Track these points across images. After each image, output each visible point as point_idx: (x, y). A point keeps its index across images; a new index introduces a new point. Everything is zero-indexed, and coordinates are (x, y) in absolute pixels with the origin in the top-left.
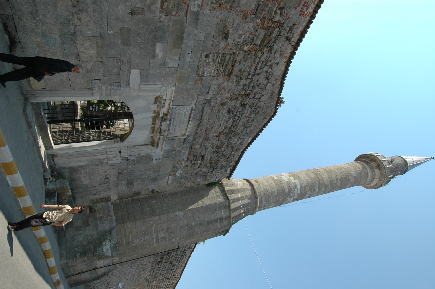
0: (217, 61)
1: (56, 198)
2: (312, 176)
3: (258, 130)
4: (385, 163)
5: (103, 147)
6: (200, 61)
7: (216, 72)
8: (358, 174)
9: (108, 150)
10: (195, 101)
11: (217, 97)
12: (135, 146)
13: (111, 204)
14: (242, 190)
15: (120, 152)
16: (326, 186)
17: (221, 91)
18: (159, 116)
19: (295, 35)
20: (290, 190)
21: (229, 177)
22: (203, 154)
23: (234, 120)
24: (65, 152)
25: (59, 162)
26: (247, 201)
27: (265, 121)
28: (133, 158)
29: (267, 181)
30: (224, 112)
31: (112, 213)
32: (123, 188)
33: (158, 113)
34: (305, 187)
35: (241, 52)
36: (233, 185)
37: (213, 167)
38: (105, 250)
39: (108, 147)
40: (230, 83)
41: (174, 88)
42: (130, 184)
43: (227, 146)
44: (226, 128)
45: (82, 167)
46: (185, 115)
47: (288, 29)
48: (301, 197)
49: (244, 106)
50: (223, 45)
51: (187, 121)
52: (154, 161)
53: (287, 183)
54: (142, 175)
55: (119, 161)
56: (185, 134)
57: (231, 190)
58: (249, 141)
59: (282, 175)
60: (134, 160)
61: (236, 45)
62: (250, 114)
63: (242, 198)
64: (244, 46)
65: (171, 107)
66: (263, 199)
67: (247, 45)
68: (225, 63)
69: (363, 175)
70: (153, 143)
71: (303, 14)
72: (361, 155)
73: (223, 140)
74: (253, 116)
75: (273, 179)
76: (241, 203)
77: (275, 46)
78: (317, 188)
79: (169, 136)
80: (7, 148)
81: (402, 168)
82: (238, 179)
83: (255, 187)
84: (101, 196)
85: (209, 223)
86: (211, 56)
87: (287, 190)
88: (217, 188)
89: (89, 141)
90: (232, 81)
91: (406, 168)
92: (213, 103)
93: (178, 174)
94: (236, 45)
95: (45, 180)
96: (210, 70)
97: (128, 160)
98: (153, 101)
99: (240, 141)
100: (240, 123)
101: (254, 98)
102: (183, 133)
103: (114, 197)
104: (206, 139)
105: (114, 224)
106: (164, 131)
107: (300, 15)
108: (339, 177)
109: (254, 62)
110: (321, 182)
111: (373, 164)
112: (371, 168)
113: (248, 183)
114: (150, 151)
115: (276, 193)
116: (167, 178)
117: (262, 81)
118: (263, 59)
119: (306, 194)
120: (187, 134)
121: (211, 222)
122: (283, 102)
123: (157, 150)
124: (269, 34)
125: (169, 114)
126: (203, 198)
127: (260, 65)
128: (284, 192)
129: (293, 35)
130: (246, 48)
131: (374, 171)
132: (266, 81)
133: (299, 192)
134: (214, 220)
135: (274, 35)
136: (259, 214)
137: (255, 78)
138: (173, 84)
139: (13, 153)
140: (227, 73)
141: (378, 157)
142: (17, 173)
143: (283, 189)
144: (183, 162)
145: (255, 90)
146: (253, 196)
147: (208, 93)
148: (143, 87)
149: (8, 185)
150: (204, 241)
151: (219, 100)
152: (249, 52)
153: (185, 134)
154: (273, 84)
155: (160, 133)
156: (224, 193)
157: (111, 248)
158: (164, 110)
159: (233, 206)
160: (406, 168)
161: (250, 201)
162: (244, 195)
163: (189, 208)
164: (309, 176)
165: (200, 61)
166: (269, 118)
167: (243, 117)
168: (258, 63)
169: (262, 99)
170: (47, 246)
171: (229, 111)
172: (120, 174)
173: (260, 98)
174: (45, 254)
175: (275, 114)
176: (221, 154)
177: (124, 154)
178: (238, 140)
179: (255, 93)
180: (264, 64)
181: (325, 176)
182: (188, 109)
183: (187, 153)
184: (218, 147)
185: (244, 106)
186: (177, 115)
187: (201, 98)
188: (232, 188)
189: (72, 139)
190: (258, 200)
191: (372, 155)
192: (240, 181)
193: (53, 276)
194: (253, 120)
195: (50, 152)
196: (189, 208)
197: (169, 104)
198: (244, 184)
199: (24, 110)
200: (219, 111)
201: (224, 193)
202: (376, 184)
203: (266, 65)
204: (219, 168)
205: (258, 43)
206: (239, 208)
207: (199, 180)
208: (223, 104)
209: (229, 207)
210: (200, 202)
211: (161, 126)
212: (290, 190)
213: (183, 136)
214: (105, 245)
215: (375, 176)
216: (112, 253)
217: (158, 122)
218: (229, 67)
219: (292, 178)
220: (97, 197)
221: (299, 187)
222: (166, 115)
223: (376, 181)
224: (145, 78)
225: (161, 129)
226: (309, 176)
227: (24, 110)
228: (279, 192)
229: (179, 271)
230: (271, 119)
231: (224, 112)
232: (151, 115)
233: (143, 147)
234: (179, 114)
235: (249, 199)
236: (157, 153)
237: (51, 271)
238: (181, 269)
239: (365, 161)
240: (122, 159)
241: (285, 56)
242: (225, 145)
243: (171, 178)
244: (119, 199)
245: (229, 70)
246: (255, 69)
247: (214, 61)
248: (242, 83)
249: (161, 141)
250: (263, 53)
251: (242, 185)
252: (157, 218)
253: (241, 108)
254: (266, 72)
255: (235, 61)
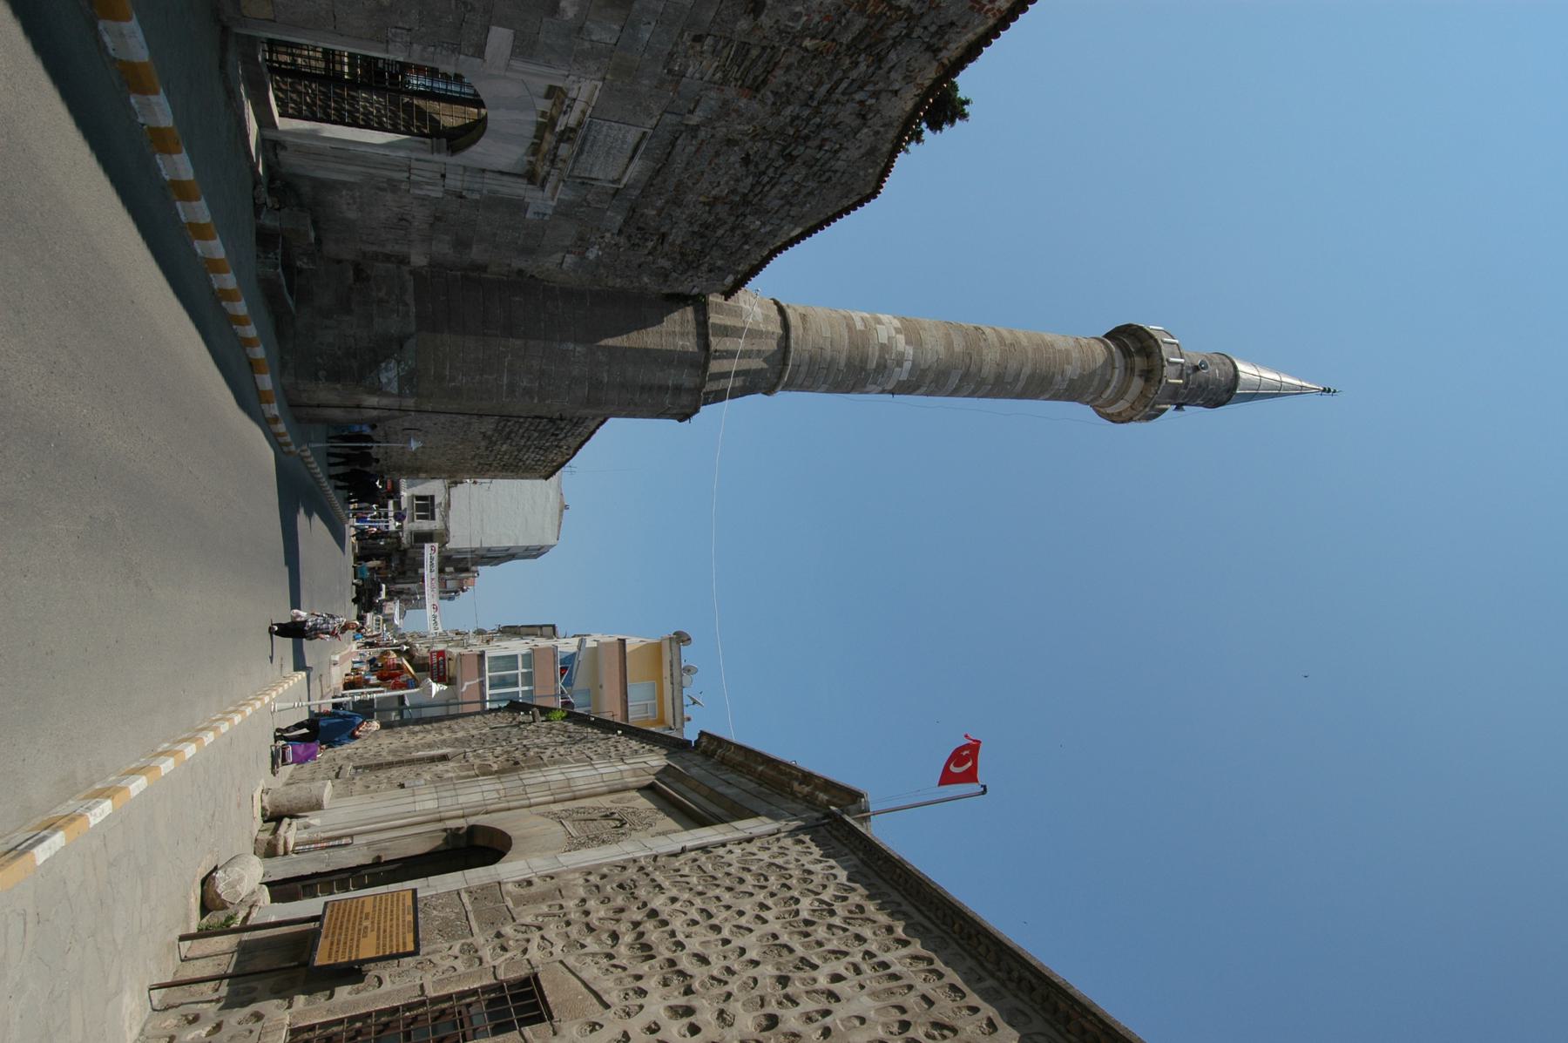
0: (725, 53)
1: (279, 251)
2: (959, 346)
3: (822, 217)
4: (1168, 370)
5: (402, 154)
6: (676, 44)
7: (719, 75)
8: (1081, 377)
9: (414, 164)
10: (654, 121)
11: (717, 124)
12: (484, 171)
13: (411, 273)
14: (754, 334)
15: (443, 176)
16: (982, 382)
17: (728, 115)
18: (554, 125)
19: (952, 46)
20: (882, 367)
21: (729, 294)
22: (663, 230)
23: (758, 183)
24: (306, 142)
25: (288, 159)
26: (757, 364)
27: (846, 203)
28: (477, 196)
29: (832, 327)
30: (732, 159)
31: (410, 298)
32: (443, 248)
33: (553, 122)
34: (924, 372)
35: (794, 49)
36: (737, 313)
37: (688, 262)
38: (384, 380)
39: (414, 155)
40: (755, 105)
41: (600, 84)
42: (462, 244)
43: (733, 229)
44: (733, 192)
45: (344, 184)
46: (623, 142)
47: (933, 29)
48: (906, 388)
49: (790, 159)
50: (744, 24)
51: (629, 153)
52: (529, 215)
53: (883, 347)
54: (495, 235)
55: (440, 195)
56: (618, 181)
57: (726, 327)
58: (794, 234)
59: (879, 322)
60: (477, 201)
61: (780, 32)
62: (806, 178)
63: (746, 354)
64: (803, 38)
65: (587, 120)
66: (804, 369)
67: (813, 37)
68: (747, 63)
69: (1095, 383)
70: (531, 177)
71: (979, 11)
72: (1130, 326)
73: (723, 215)
74: (812, 184)
75: (850, 327)
76: (734, 365)
77: (893, 56)
78: (954, 380)
79: (576, 173)
80: (202, 203)
81: (1217, 390)
82: (753, 304)
83: (793, 335)
84: (388, 249)
85: (644, 388)
86: (709, 41)
87: (872, 365)
88: (689, 313)
89: (368, 126)
90: (762, 101)
91: (1225, 396)
92: (702, 134)
93: (592, 254)
94: (780, 32)
95: (258, 209)
96: (701, 68)
97: (461, 197)
98: (543, 91)
99: (768, 228)
100: (774, 191)
101: (820, 147)
102: (614, 175)
103: (418, 259)
104: (677, 202)
105: (413, 328)
106: (564, 161)
107: (972, 8)
108: (1027, 370)
109: (830, 74)
110: (973, 369)
111: (1139, 362)
112: (1129, 370)
113: (779, 318)
114: (521, 192)
115: (843, 363)
116: (560, 255)
117: (846, 115)
118: (854, 74)
119: (919, 387)
120: (624, 181)
121: (651, 388)
122: (964, 116)
123: (540, 194)
124: (877, 28)
125: (581, 132)
126: (645, 327)
127: (844, 85)
128: (863, 369)
129: (948, 43)
130: (807, 43)
131: (1130, 382)
132: (858, 121)
133: (904, 377)
134: (660, 387)
135: (892, 33)
136: (781, 397)
137: (828, 110)
138: (599, 75)
139: (194, 166)
140: (749, 82)
141: (1163, 347)
142: (129, 19)
143: (864, 360)
144: (608, 235)
145: (826, 134)
146: (779, 356)
147: (691, 112)
148: (516, 64)
149: (196, 254)
150: (943, 108)
151: (721, 131)
152: (817, 53)
153: (618, 181)
154: (877, 133)
155: (553, 162)
156: (703, 330)
157: (400, 378)
158: (571, 119)
159: (715, 366)
160: (1225, 396)
161: (765, 366)
162: (755, 348)
163: (603, 343)
164: (949, 345)
165: (676, 44)
166: (856, 199)
167: (783, 180)
168: (841, 80)
169: (842, 155)
170: (259, 352)
171: (746, 160)
172: (438, 219)
173: (836, 152)
174: (253, 366)
175: (874, 194)
176: (713, 241)
177: (454, 182)
178: (764, 224)
179: (824, 140)
180: (855, 85)
181: (991, 356)
182: (633, 136)
183: (619, 219)
184: (706, 226)
185: (790, 159)
186: (601, 137)
187: (669, 119)
188: (729, 321)
189: (325, 108)
190: (781, 368)
191: (1151, 336)
192: (761, 306)
193: (264, 406)
194: (811, 193)
195: (269, 134)
196: (603, 343)
197: (584, 112)
198: (766, 318)
199: (222, 65)
200: (717, 154)
201: (703, 330)
202: (1120, 414)
203: (861, 88)
204: (705, 268)
205: (846, 39)
206: (726, 375)
207: (646, 280)
208: (730, 142)
209: (705, 367)
210: (634, 335)
211: (556, 148)
212: (882, 367)
213: (613, 182)
214: (387, 370)
215: (1125, 393)
216: (400, 388)
217: (549, 139)
218: (758, 70)
219: (901, 338)
220: (374, 248)
221: (907, 365)
222: (573, 130)
223: (1122, 405)
224: (524, 48)
225: (555, 155)
226: (949, 345)
227: (222, 65)
228: (849, 364)
229: (573, 442)
230: (861, 203)
231: (732, 159)
232: (534, 117)
233: (505, 178)
234: (607, 135)
235: (765, 360)
236: (540, 201)
237: (263, 397)
238: (579, 440)
239: (1126, 346)
240: (446, 192)
241: (919, 81)
242: (727, 227)
243: (570, 259)
244: (430, 265)
245: (756, 78)
246: (830, 91)
247: (715, 52)
248: (788, 111)
249: (552, 179)
250: (856, 64)
251: (760, 318)
252: (519, 342)
253: (781, 162)
254: (862, 103)
255: (776, 64)
